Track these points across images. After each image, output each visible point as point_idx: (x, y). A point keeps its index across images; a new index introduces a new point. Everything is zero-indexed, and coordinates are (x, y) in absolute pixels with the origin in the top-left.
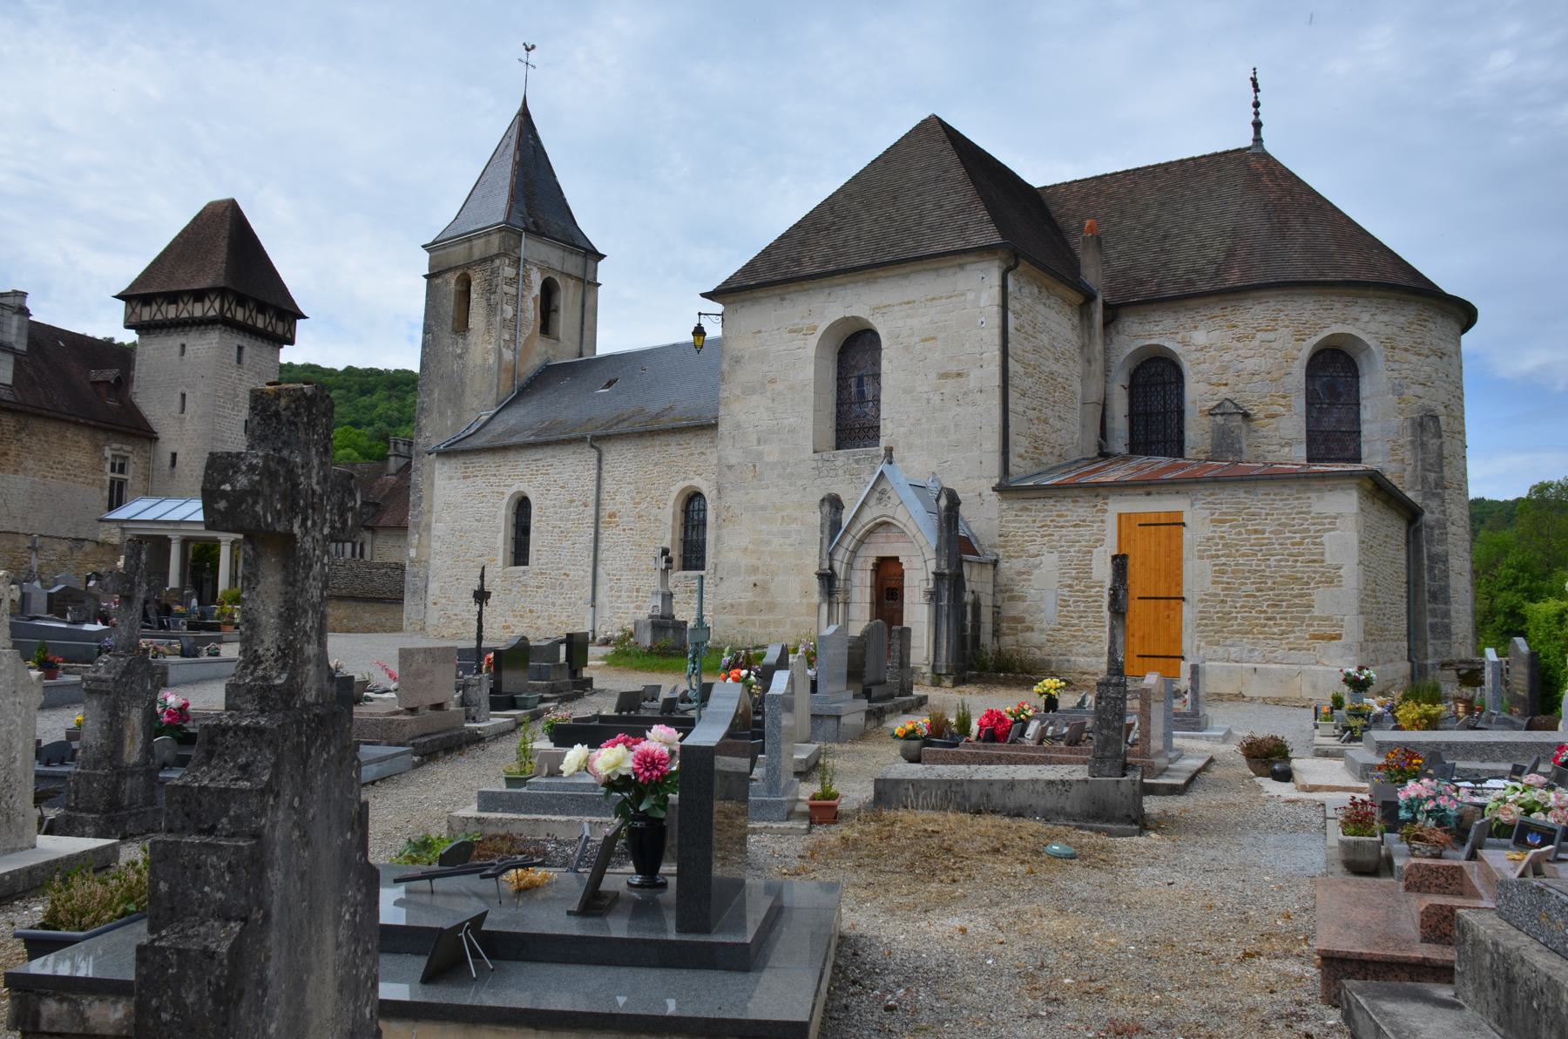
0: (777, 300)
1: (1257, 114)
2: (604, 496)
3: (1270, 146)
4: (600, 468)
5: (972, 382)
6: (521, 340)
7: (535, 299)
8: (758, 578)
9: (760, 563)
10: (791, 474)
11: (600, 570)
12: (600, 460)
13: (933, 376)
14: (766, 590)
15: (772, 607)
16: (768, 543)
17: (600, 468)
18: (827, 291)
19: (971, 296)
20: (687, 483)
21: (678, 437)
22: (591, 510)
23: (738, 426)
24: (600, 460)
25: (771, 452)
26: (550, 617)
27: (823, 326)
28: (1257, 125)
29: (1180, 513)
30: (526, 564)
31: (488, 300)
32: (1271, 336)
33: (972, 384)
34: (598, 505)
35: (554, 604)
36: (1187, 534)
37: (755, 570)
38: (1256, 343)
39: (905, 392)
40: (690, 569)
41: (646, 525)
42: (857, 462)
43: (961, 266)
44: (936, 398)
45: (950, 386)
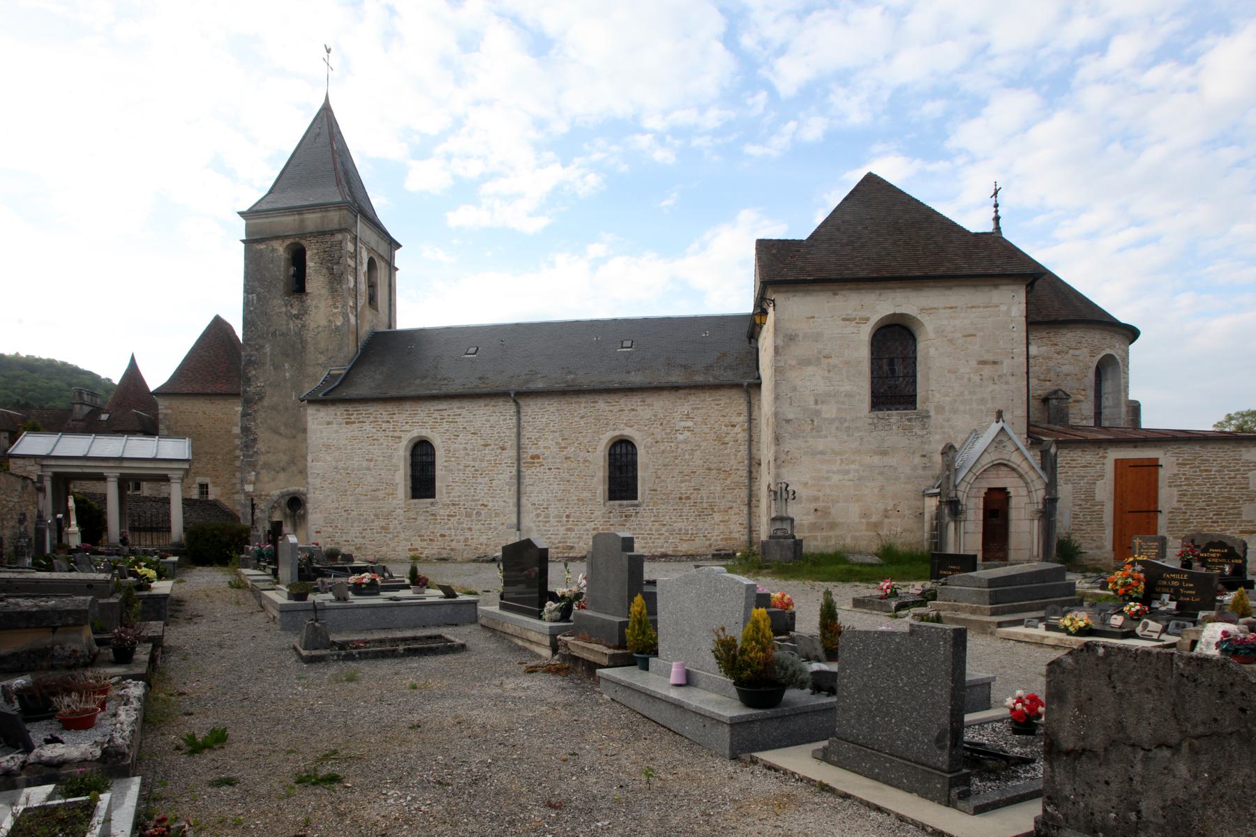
0: (830, 294)
1: (996, 212)
2: (524, 441)
3: (1007, 234)
4: (519, 419)
5: (1005, 368)
8: (819, 505)
10: (849, 428)
11: (524, 500)
12: (518, 412)
13: (973, 363)
15: (833, 526)
17: (519, 419)
18: (878, 292)
19: (1003, 308)
20: (617, 433)
21: (606, 397)
23: (795, 389)
24: (518, 412)
25: (829, 411)
26: (466, 540)
27: (875, 318)
28: (997, 219)
29: (1157, 459)
31: (330, 270)
32: (1077, 352)
34: (519, 448)
35: (470, 529)
36: (1161, 472)
37: (816, 499)
38: (1069, 355)
39: (949, 372)
40: (615, 499)
41: (573, 465)
42: (909, 420)
43: (996, 286)
44: (976, 378)
45: (987, 371)
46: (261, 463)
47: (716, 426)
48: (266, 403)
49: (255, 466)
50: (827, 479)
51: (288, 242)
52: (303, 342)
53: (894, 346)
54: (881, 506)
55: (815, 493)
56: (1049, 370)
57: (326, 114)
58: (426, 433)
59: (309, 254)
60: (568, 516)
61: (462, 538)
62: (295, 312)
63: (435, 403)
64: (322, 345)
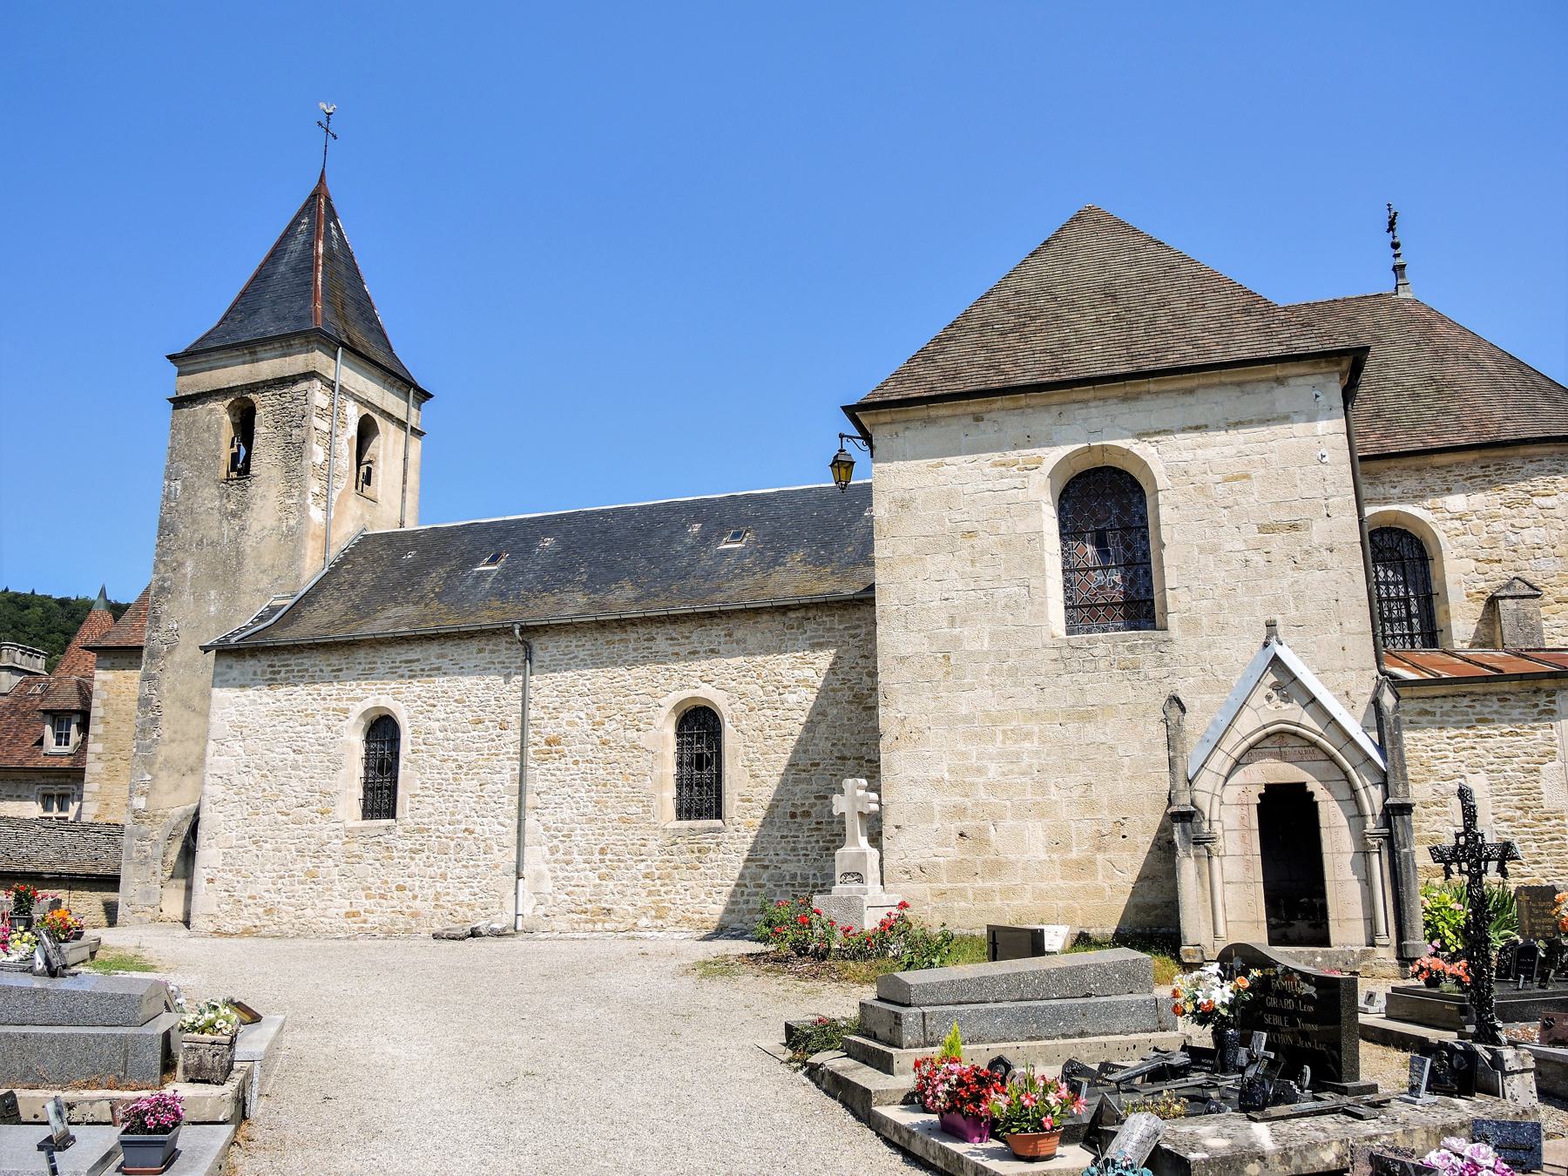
5: (1319, 532)
6: (335, 496)
7: (350, 442)
8: (967, 824)
9: (968, 802)
14: (982, 841)
15: (996, 868)
16: (980, 771)
21: (670, 630)
22: (513, 735)
25: (976, 638)
30: (392, 814)
32: (1548, 502)
33: (1316, 541)
37: (960, 812)
39: (1202, 550)
42: (1131, 649)
45: (1277, 541)
46: (161, 759)
47: (853, 675)
48: (177, 657)
49: (151, 765)
50: (980, 771)
51: (366, 411)
52: (239, 554)
53: (1106, 508)
54: (1088, 828)
55: (958, 799)
56: (1494, 543)
57: (318, 208)
58: (707, 693)
59: (260, 412)
60: (602, 851)
61: (431, 892)
62: (232, 506)
63: (399, 649)
64: (267, 560)
